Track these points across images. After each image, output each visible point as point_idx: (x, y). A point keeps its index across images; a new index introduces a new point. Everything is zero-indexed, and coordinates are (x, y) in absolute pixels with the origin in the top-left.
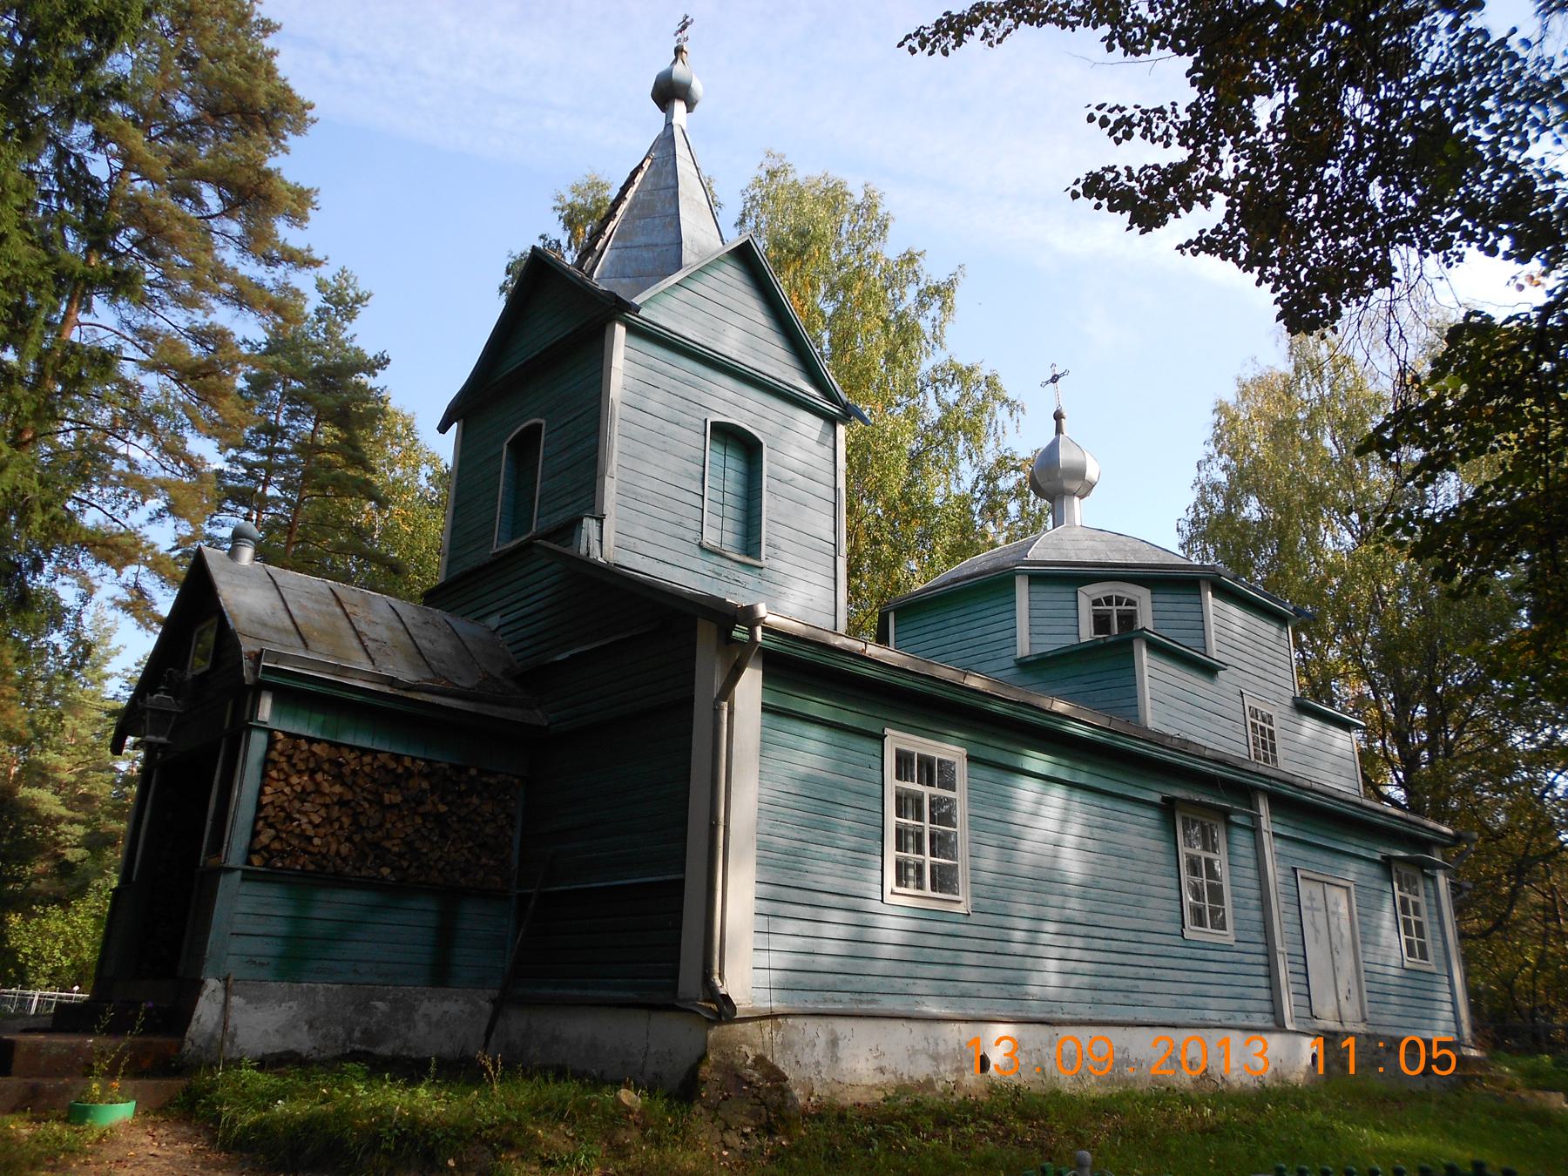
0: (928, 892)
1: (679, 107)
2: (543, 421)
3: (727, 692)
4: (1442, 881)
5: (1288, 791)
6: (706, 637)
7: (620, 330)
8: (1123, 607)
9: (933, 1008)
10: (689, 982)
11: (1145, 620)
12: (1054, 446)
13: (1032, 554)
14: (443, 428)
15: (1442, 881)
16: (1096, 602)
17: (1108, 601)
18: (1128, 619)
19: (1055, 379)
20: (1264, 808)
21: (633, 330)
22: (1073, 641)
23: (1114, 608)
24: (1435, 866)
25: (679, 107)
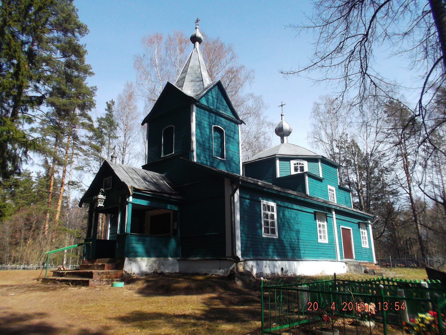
0: (270, 234)
1: (197, 43)
2: (351, 229)
3: (233, 195)
4: (370, 226)
5: (338, 208)
6: (227, 182)
7: (195, 108)
8: (301, 165)
9: (277, 258)
10: (228, 253)
11: (306, 170)
12: (282, 122)
13: (206, 85)
14: (143, 124)
15: (370, 226)
16: (295, 164)
17: (297, 164)
18: (302, 169)
19: (282, 106)
20: (334, 213)
21: (197, 106)
22: (288, 174)
23: (299, 165)
24: (369, 224)
25: (197, 43)
